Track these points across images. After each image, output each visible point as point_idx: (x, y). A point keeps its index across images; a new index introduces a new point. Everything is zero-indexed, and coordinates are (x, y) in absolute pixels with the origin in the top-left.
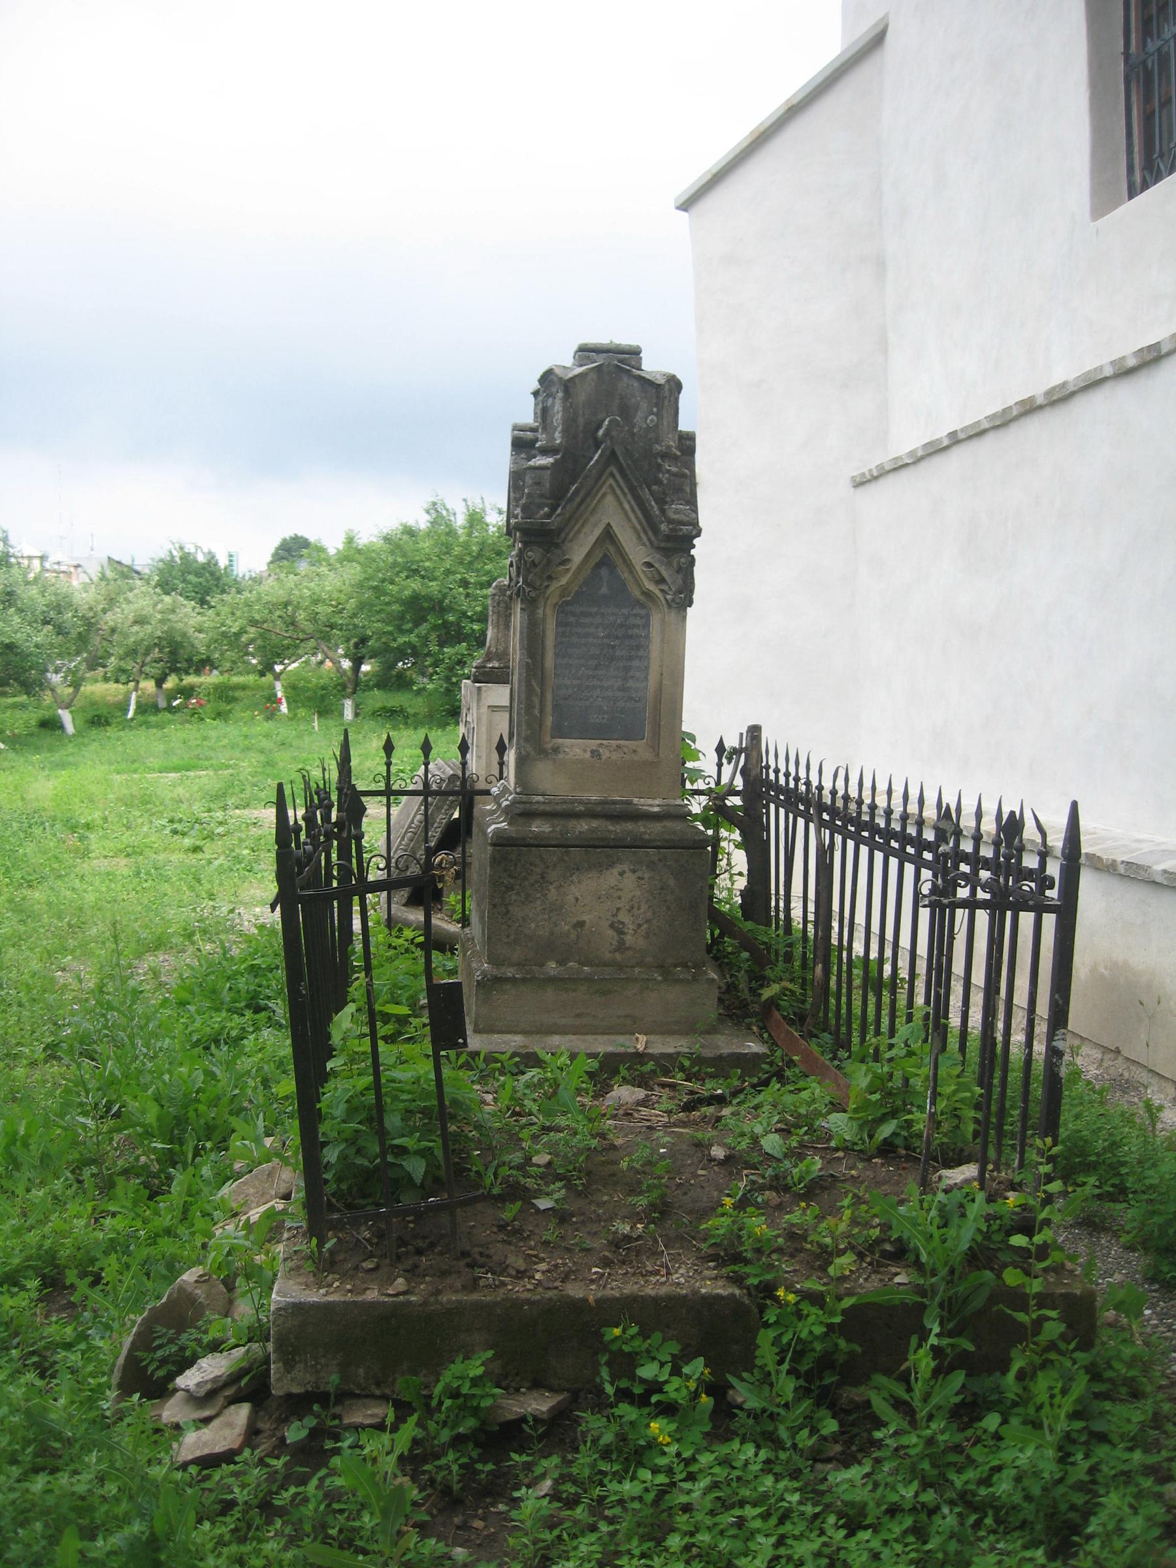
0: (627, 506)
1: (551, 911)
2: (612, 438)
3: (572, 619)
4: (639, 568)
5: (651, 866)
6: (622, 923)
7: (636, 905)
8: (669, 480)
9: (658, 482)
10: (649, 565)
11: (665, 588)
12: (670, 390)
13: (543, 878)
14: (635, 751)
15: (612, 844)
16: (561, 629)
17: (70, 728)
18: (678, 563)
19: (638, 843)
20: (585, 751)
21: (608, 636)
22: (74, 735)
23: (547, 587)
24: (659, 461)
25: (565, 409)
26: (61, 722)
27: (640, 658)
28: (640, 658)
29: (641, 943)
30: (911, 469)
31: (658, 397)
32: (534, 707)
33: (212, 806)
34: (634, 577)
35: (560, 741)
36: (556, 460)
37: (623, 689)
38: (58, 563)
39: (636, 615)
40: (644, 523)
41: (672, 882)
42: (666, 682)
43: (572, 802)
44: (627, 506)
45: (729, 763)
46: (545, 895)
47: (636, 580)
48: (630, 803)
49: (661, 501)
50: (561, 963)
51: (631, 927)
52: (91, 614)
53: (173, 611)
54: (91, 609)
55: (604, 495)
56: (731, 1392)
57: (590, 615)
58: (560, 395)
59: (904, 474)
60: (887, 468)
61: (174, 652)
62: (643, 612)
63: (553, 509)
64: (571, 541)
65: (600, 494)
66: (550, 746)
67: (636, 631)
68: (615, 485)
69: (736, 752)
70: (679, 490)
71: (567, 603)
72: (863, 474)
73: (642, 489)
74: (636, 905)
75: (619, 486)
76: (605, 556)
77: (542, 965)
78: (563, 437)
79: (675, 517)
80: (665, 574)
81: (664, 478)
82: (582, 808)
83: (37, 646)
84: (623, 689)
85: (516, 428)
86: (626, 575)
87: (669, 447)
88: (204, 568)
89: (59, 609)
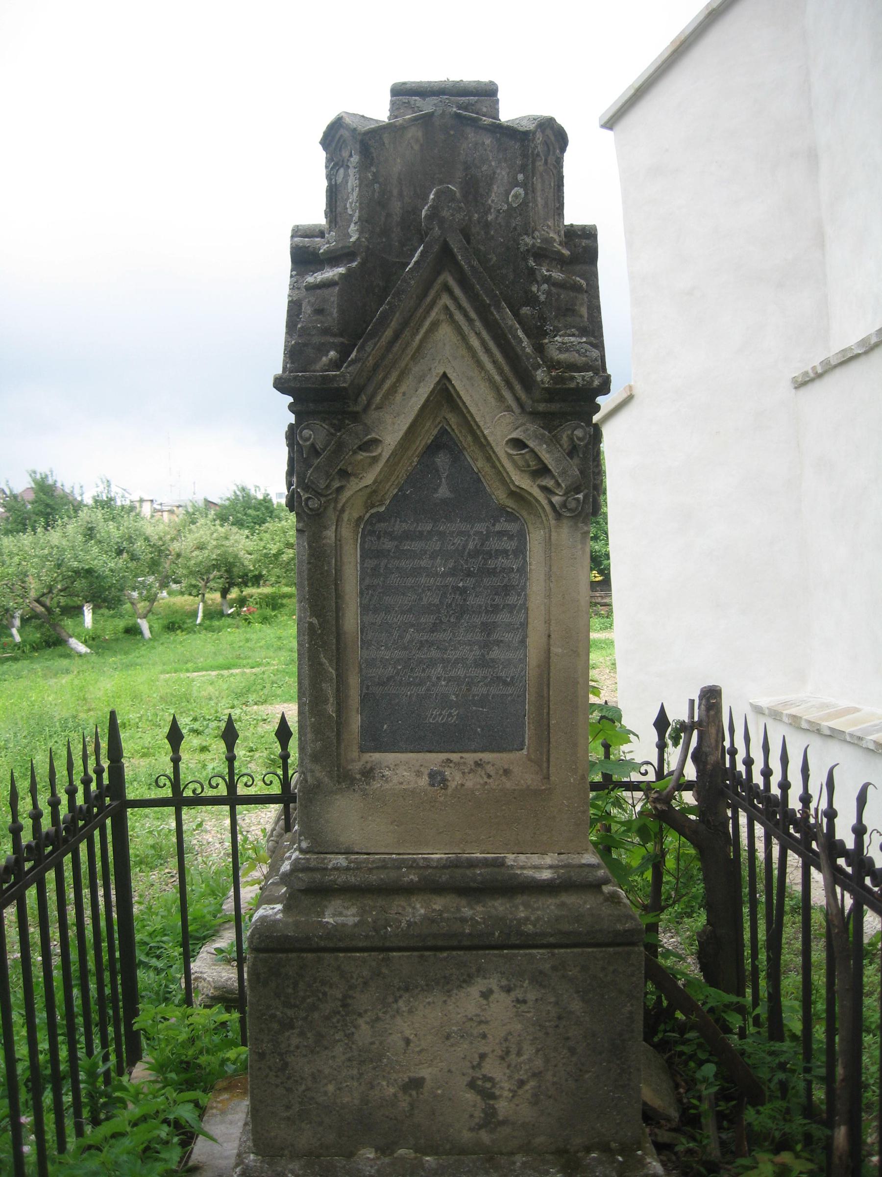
0: (475, 343)
1: (362, 1062)
2: (442, 221)
3: (388, 545)
4: (501, 450)
5: (539, 979)
6: (491, 1079)
7: (514, 1049)
8: (548, 293)
9: (531, 300)
10: (518, 444)
11: (549, 483)
12: (546, 143)
13: (345, 1006)
14: (506, 772)
15: (466, 943)
16: (370, 563)
17: (147, 634)
18: (571, 439)
19: (514, 940)
20: (419, 774)
21: (453, 572)
22: (150, 639)
23: (340, 490)
24: (531, 263)
25: (363, 184)
26: (141, 629)
27: (511, 608)
28: (511, 608)
29: (526, 1112)
30: (863, 359)
31: (525, 155)
32: (326, 701)
33: (236, 702)
34: (494, 466)
35: (376, 756)
36: (349, 270)
37: (483, 663)
38: (161, 504)
39: (501, 534)
40: (506, 369)
41: (576, 1006)
42: (556, 650)
43: (398, 865)
44: (475, 343)
45: (676, 744)
46: (350, 1036)
47: (499, 473)
48: (499, 864)
49: (537, 333)
50: (384, 1150)
51: (506, 1085)
52: (161, 543)
53: (227, 538)
54: (160, 539)
55: (435, 325)
56: (673, 735)
57: (420, 536)
58: (355, 159)
59: (854, 368)
60: (834, 362)
61: (228, 571)
62: (513, 527)
63: (344, 353)
64: (379, 408)
65: (427, 324)
66: (356, 767)
67: (501, 562)
68: (452, 307)
69: (685, 728)
70: (569, 310)
71: (379, 517)
72: (806, 373)
73: (498, 308)
74: (514, 1049)
75: (460, 307)
76: (443, 432)
77: (350, 1155)
78: (361, 231)
79: (562, 357)
80: (547, 458)
81: (540, 291)
82: (414, 877)
83: (112, 570)
84: (483, 663)
85: (297, 232)
86: (481, 466)
87: (548, 241)
88: (260, 504)
89: (130, 540)
